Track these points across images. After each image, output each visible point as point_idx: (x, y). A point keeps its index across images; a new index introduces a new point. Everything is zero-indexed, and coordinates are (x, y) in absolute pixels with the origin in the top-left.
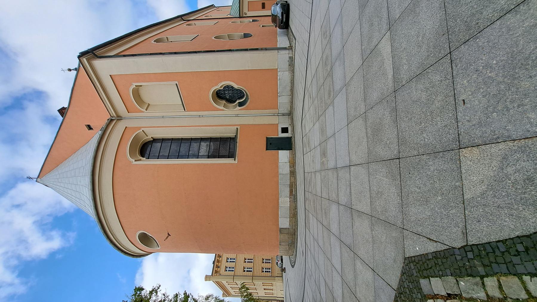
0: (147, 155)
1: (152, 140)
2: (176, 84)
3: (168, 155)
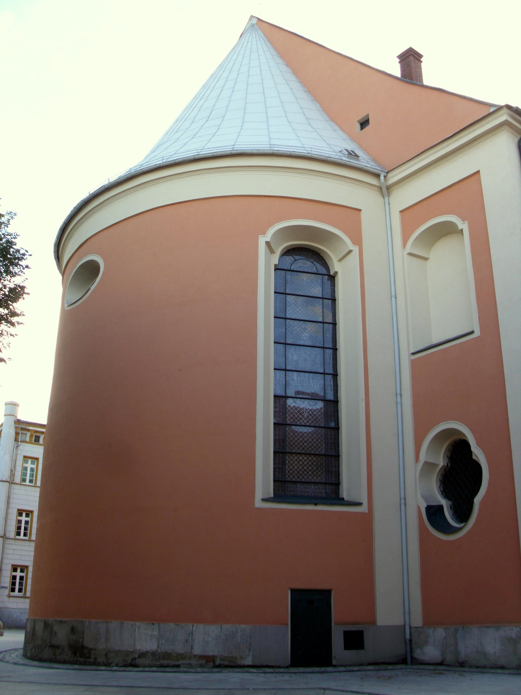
0: (17, 426)
1: (332, 273)
2: (472, 332)
3: (288, 316)
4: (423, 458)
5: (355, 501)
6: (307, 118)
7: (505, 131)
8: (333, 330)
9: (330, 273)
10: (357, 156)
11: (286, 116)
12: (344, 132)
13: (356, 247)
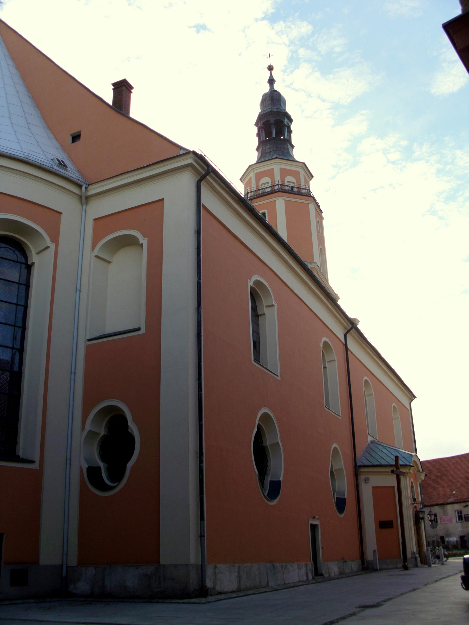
1: (29, 263)
2: (139, 329)
4: (88, 427)
5: (30, 459)
6: (28, 123)
7: (188, 172)
8: (24, 311)
9: (27, 262)
10: (66, 166)
11: (10, 118)
12: (57, 141)
13: (54, 244)
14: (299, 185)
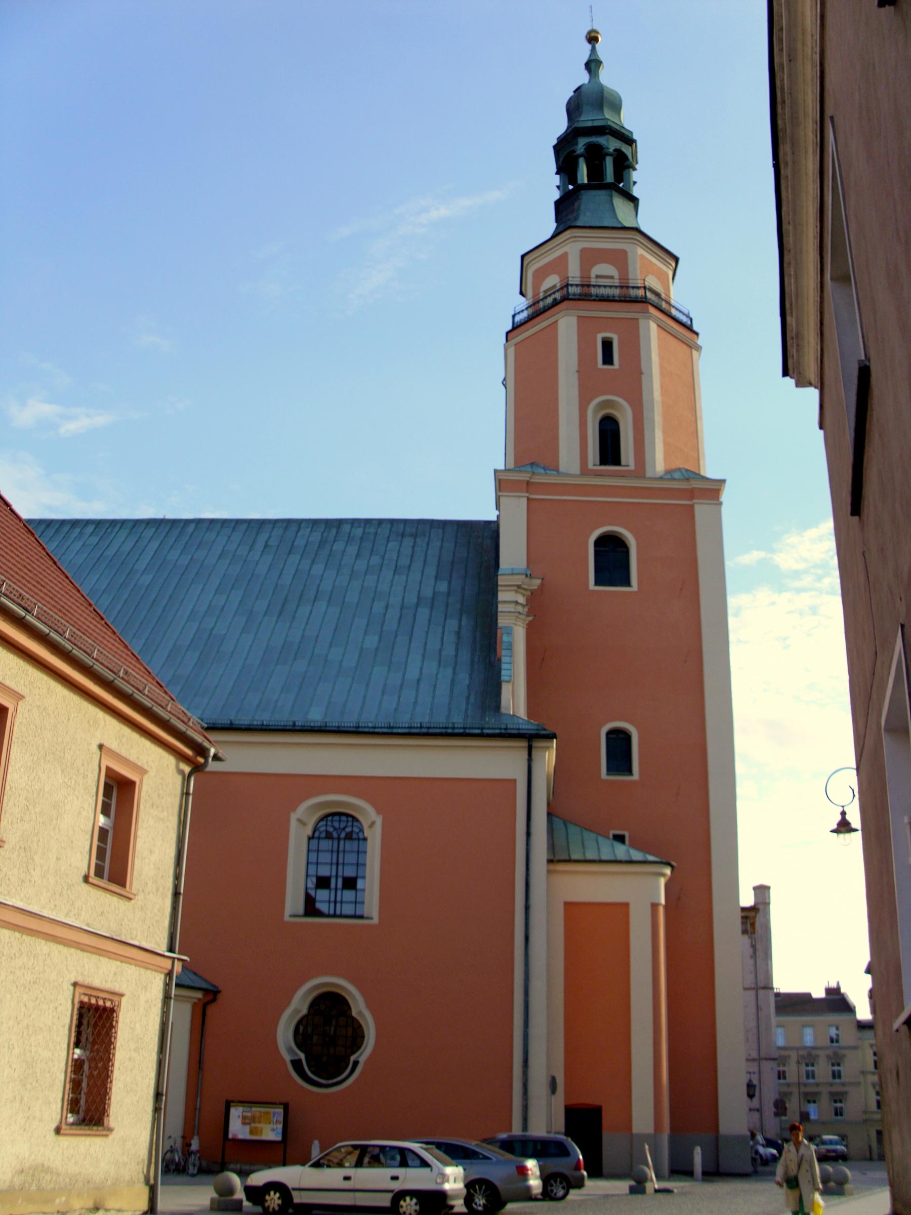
14: (623, 281)
